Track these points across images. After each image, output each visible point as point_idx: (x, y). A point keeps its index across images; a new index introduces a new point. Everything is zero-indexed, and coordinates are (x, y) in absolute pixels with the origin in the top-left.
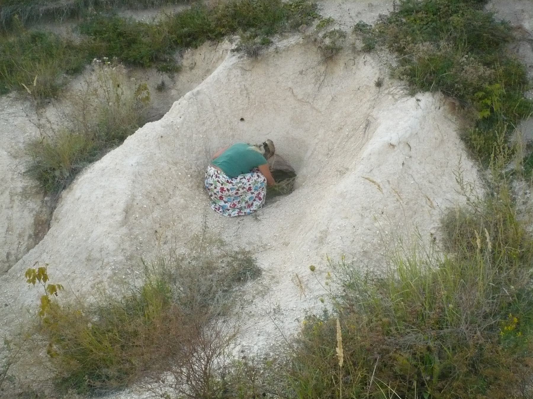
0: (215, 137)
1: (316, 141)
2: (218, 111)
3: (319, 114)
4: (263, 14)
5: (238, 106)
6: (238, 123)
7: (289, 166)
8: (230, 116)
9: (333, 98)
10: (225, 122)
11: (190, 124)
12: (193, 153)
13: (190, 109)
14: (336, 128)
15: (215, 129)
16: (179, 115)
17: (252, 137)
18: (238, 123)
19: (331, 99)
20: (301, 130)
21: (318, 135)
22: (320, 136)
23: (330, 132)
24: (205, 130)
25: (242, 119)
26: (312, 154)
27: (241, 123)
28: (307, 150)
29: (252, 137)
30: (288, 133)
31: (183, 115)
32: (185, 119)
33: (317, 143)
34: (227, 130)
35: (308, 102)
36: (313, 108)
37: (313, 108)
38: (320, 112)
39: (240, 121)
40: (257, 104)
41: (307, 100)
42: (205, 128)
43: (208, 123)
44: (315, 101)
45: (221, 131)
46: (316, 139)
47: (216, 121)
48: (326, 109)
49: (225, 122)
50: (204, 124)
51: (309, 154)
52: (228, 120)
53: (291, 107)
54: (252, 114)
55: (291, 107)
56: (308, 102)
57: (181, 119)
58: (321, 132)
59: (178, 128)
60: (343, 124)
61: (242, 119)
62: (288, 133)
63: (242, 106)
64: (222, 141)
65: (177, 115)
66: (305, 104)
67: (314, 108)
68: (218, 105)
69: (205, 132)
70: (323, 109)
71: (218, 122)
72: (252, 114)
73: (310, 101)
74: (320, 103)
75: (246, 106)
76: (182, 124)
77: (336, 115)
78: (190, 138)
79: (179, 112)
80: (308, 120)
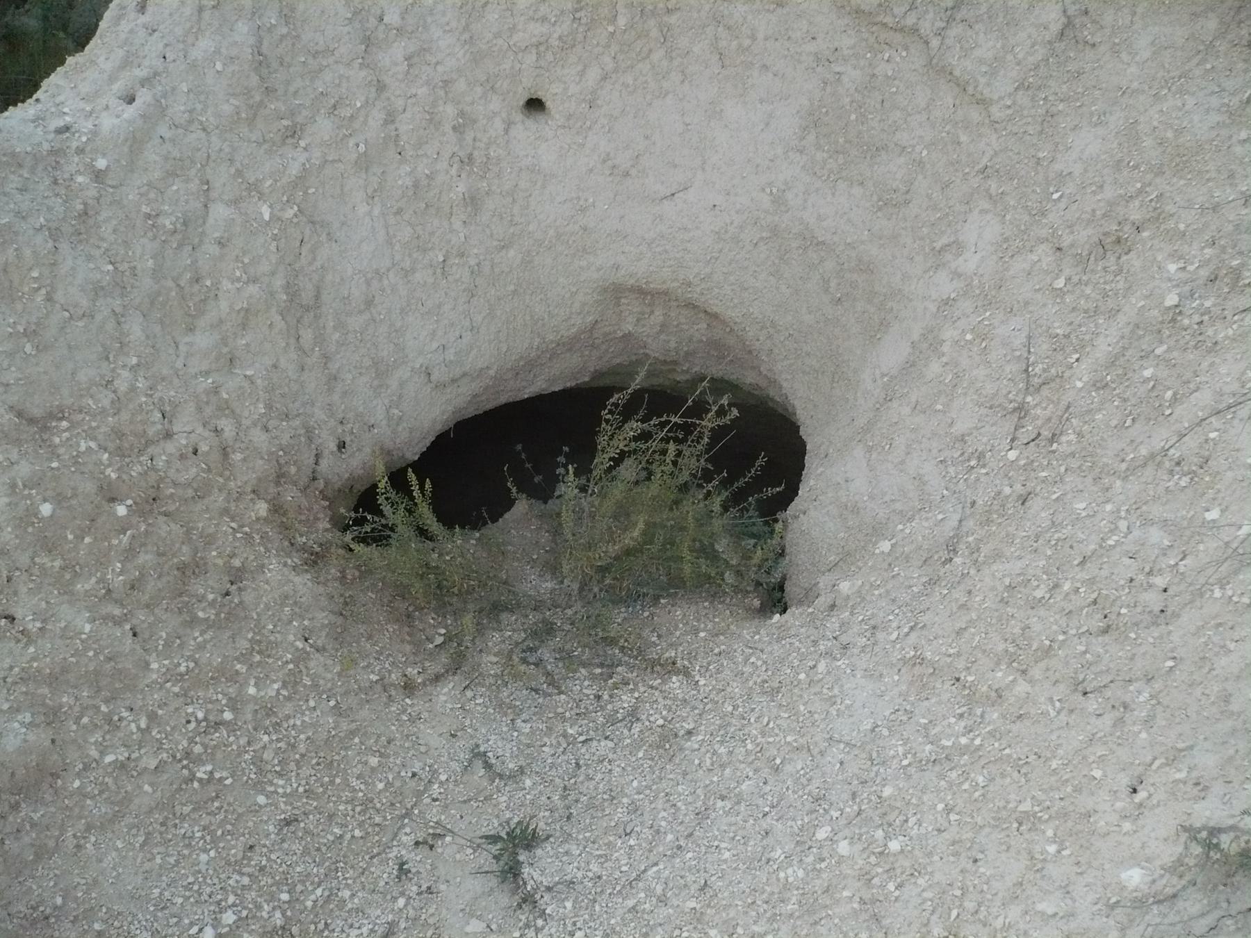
0: (363, 209)
1: (944, 286)
2: (393, 56)
3: (975, 115)
4: (1017, 630)
5: (513, 29)
6: (509, 125)
7: (773, 382)
8: (461, 85)
9: (1069, 24)
10: (433, 121)
11: (196, 136)
12: (201, 323)
13: (205, 44)
14: (1085, 236)
15: (364, 163)
16: (118, 86)
17: (583, 210)
18: (509, 125)
19: (1055, 28)
20: (857, 191)
21: (958, 247)
22: (969, 263)
23: (1043, 255)
24: (294, 170)
25: (535, 105)
26: (910, 367)
27: (526, 128)
28: (884, 325)
29: (583, 210)
30: (779, 201)
31: (144, 82)
32: (159, 109)
33: (947, 302)
34: (442, 165)
35: (915, 30)
36: (938, 70)
37: (938, 70)
38: (983, 102)
39: (518, 117)
40: (622, 21)
41: (910, 20)
42: (295, 160)
43: (324, 127)
44: (955, 31)
45: (401, 176)
46: (942, 277)
47: (377, 116)
48: (1022, 86)
49: (433, 121)
50: (293, 133)
51: (891, 354)
52: (450, 110)
53: (811, 47)
54: (593, 74)
55: (811, 47)
56: (915, 30)
57: (130, 112)
58: (981, 232)
59: (98, 176)
60: (1136, 216)
61: (535, 105)
62: (779, 201)
63: (537, 29)
64: (406, 233)
65: (112, 79)
66: (898, 37)
67: (946, 72)
68: (392, 18)
69: (301, 181)
70: (1002, 86)
71: (390, 119)
72: (593, 74)
73: (926, 27)
74: (987, 46)
75: (565, 27)
76: (135, 142)
77: (1087, 144)
78: (188, 230)
79: (126, 63)
80: (903, 137)
